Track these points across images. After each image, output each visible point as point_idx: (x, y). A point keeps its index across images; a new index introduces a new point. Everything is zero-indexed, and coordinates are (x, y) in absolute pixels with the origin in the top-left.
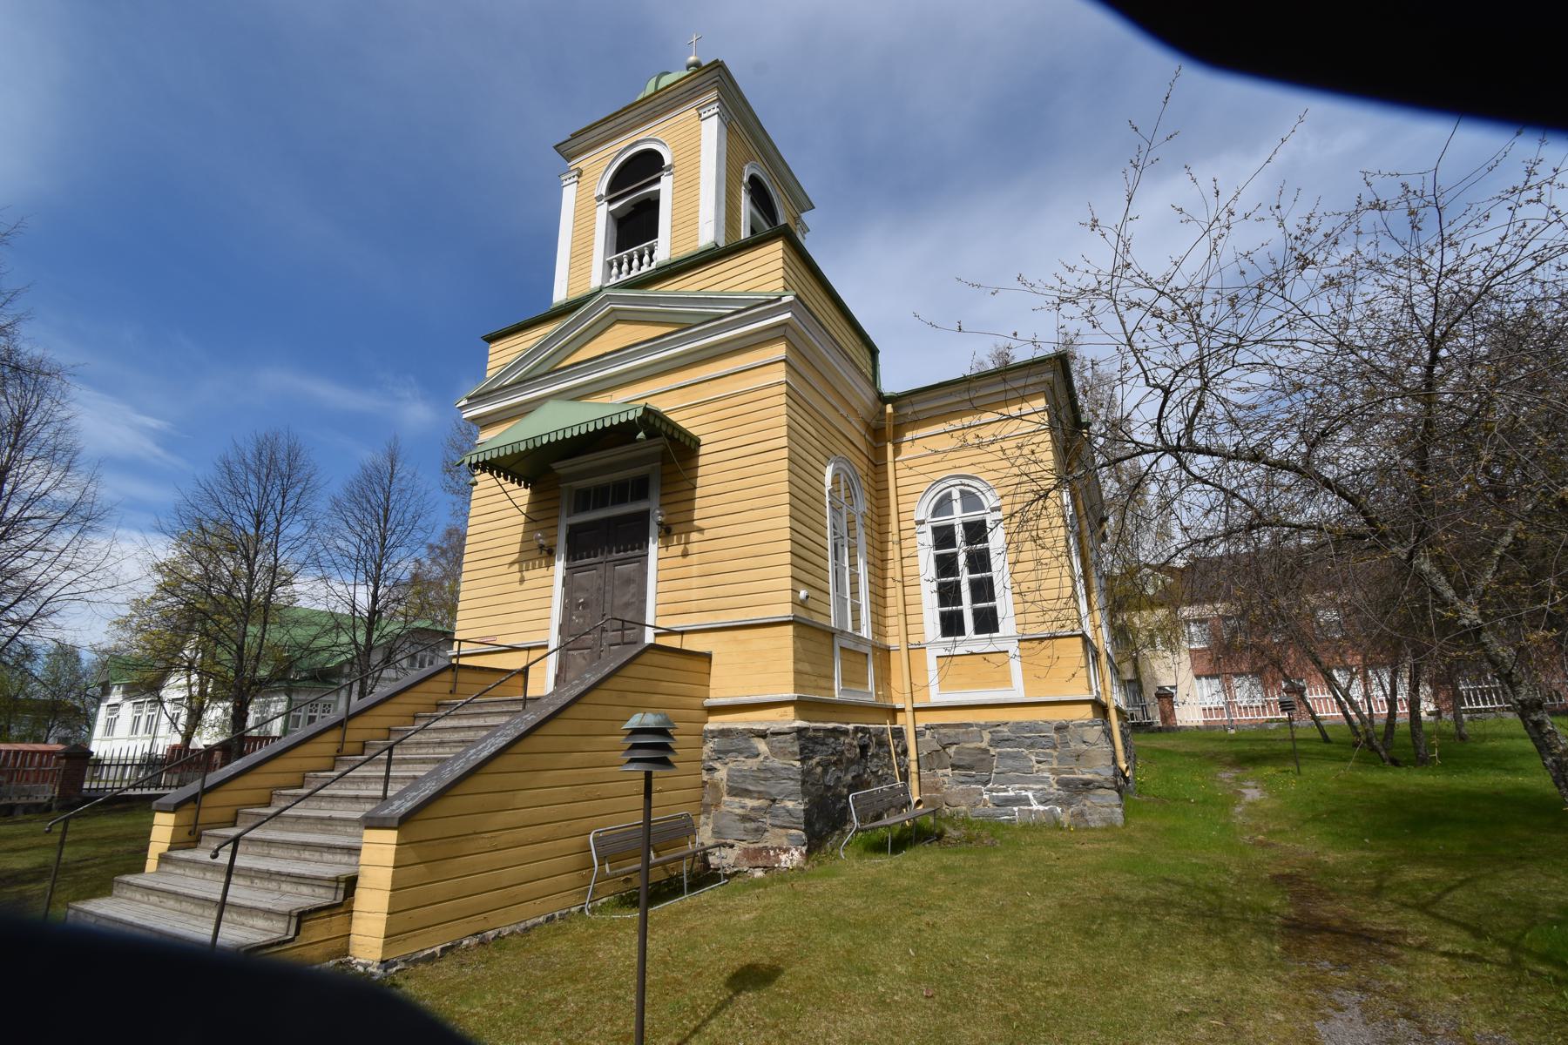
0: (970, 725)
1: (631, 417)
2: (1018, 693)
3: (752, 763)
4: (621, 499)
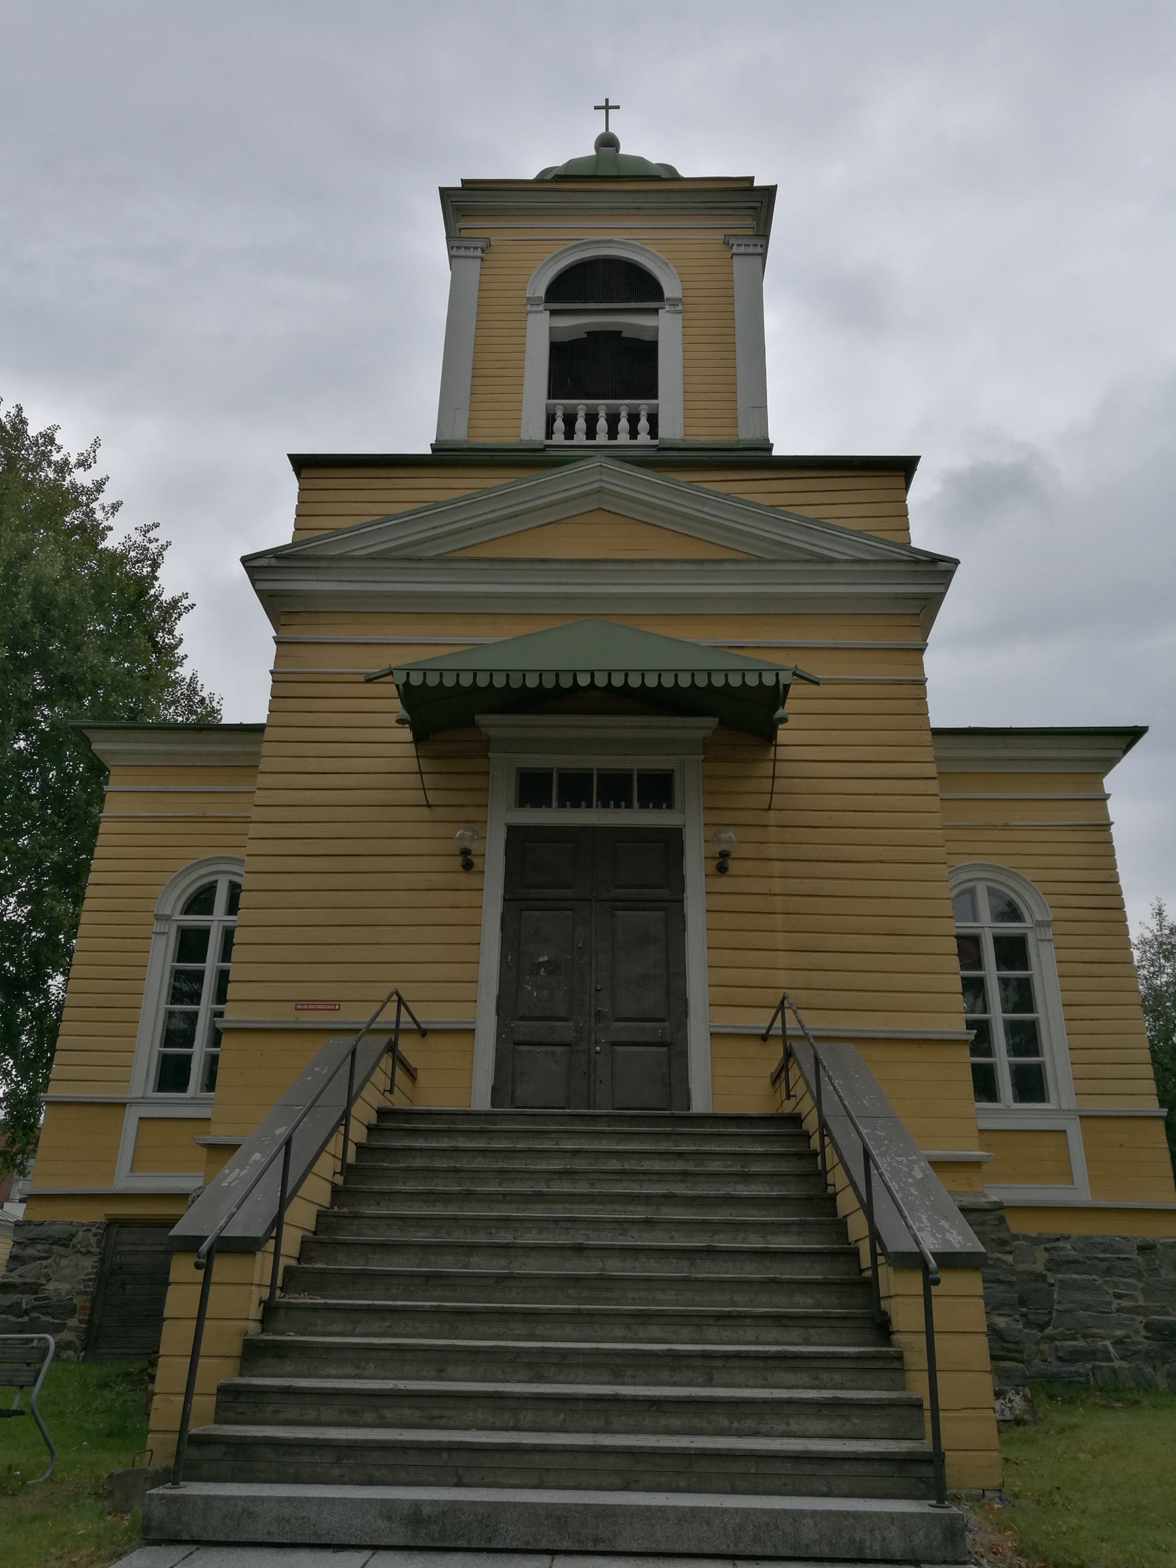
2: (1081, 1193)
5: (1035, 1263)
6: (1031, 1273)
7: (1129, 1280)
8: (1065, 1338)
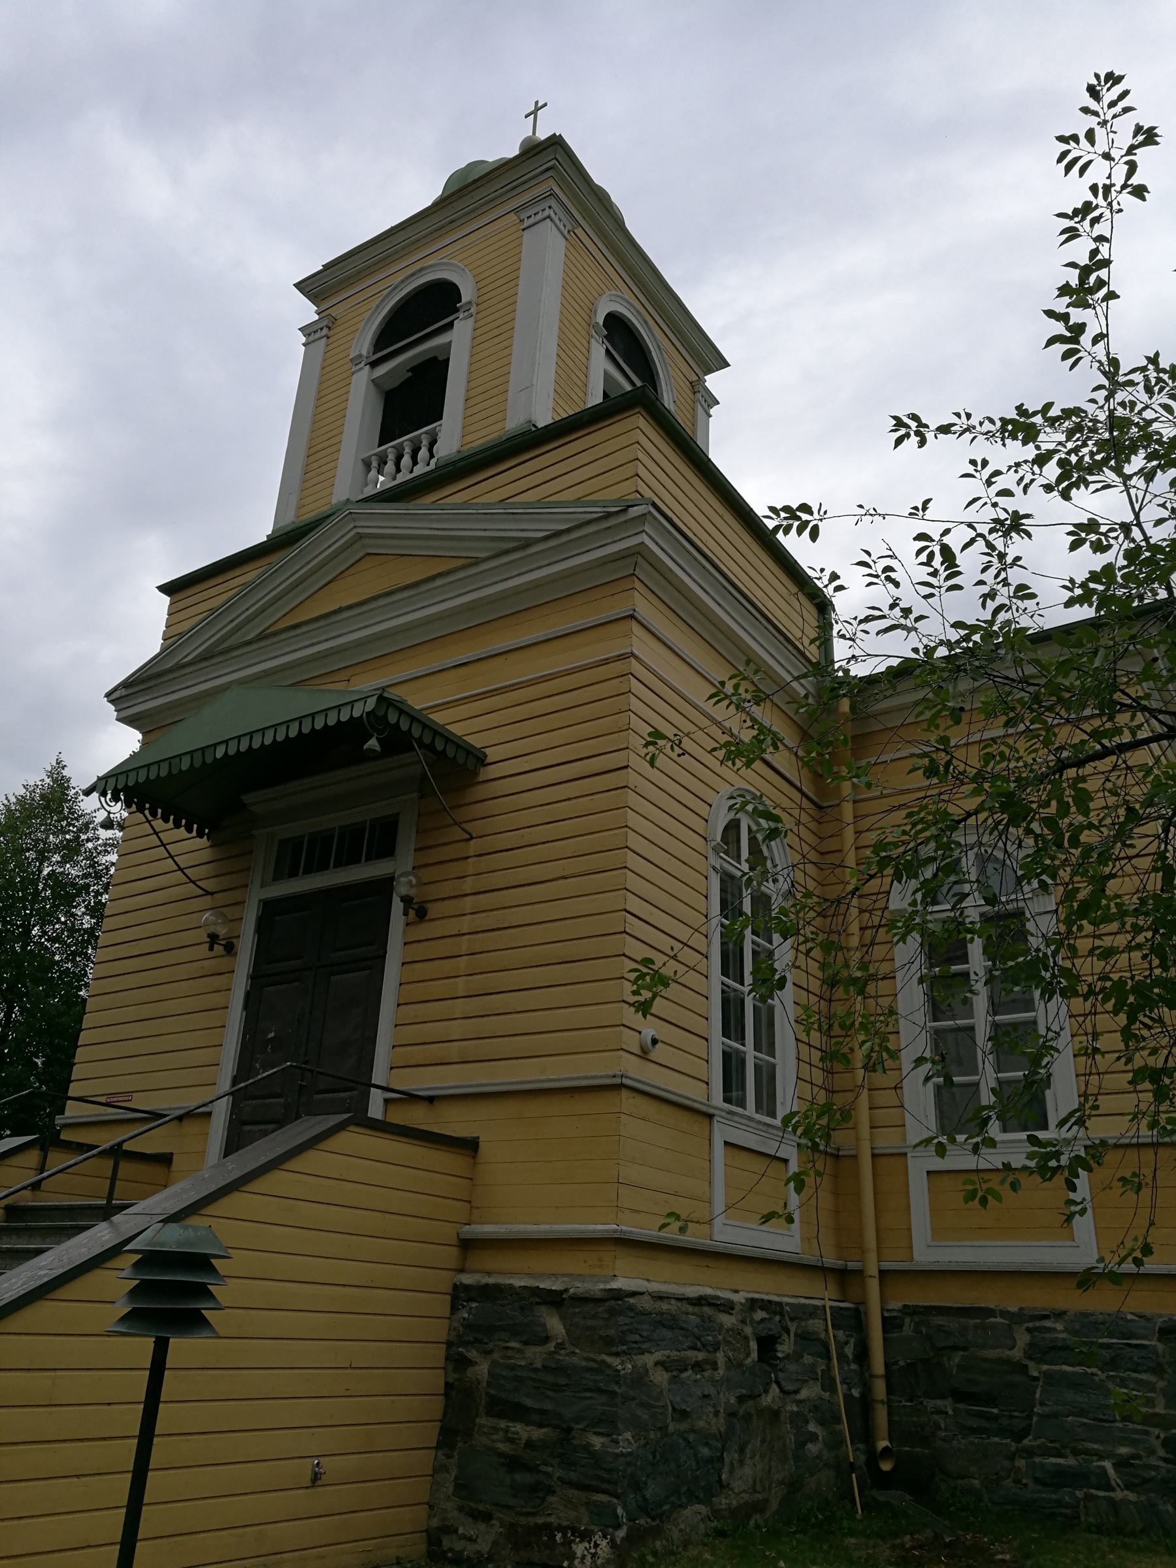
0: (990, 1312)
1: (356, 714)
3: (536, 1354)
4: (351, 858)
5: (1012, 1348)
6: (1007, 1362)
7: (1144, 1376)
8: (1046, 1452)
